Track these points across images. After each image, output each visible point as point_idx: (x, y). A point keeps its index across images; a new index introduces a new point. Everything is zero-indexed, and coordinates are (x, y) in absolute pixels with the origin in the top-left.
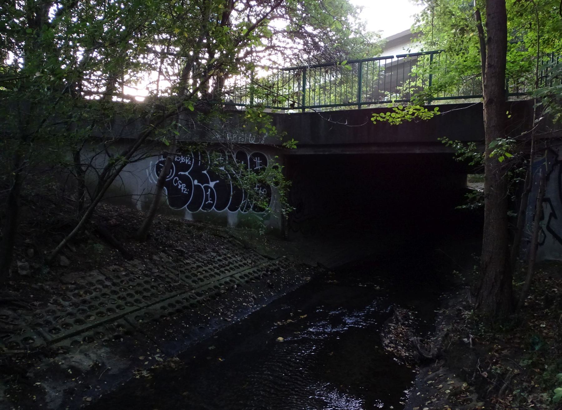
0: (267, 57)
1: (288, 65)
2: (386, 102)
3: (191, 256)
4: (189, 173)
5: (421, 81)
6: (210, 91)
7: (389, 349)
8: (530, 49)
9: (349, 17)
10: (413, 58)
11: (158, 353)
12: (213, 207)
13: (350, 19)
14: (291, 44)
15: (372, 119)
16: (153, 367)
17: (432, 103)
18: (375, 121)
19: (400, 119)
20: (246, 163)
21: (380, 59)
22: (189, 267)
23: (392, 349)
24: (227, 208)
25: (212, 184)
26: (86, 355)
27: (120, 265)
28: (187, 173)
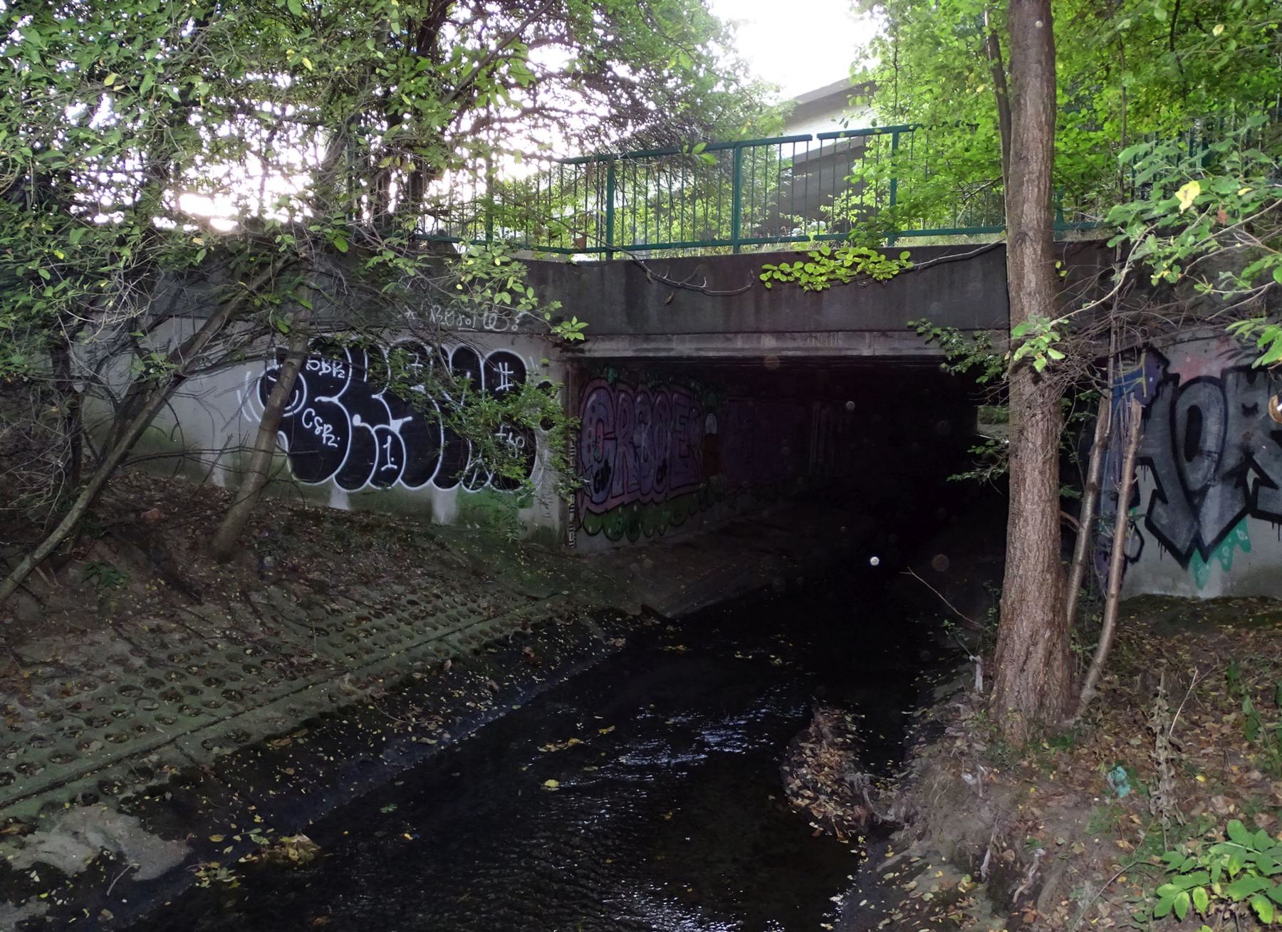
0: (525, 133)
1: (575, 153)
2: (795, 240)
3: (344, 594)
4: (341, 399)
5: (874, 194)
6: (391, 208)
7: (799, 801)
8: (1107, 126)
9: (711, 44)
10: (857, 145)
11: (257, 825)
12: (399, 479)
13: (714, 48)
14: (581, 104)
15: (764, 277)
16: (242, 860)
17: (898, 244)
18: (769, 280)
19: (824, 278)
20: (476, 375)
21: (781, 141)
22: (338, 620)
23: (807, 801)
24: (431, 480)
25: (395, 425)
26: (75, 834)
27: (171, 617)
28: (335, 400)
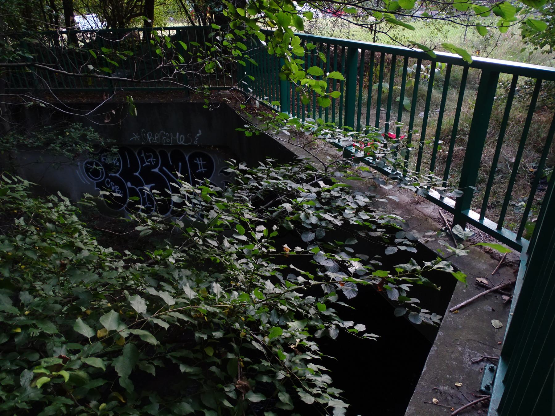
4: (120, 175)
24: (169, 213)
28: (117, 175)
